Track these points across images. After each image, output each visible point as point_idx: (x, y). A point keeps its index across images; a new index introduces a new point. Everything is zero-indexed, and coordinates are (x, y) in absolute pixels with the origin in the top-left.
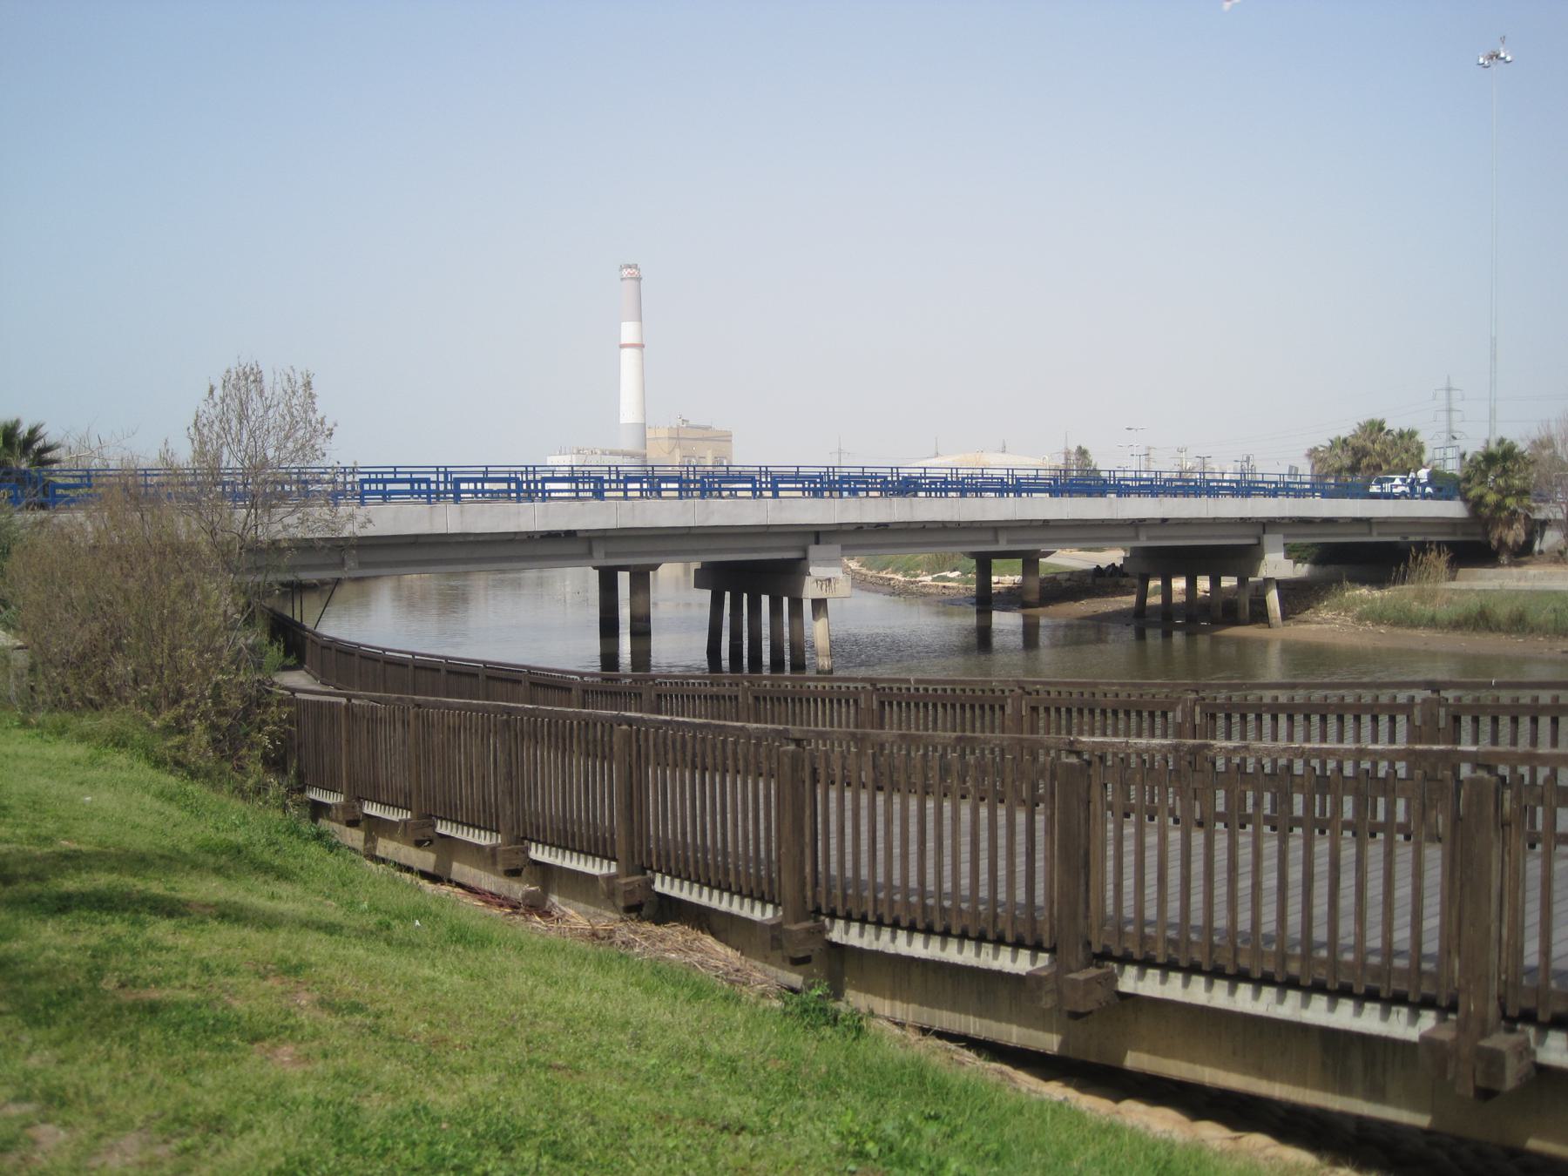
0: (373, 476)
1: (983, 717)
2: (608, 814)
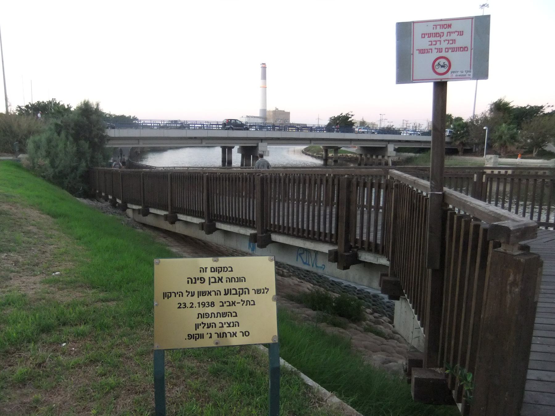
0: (192, 123)
2: (255, 216)
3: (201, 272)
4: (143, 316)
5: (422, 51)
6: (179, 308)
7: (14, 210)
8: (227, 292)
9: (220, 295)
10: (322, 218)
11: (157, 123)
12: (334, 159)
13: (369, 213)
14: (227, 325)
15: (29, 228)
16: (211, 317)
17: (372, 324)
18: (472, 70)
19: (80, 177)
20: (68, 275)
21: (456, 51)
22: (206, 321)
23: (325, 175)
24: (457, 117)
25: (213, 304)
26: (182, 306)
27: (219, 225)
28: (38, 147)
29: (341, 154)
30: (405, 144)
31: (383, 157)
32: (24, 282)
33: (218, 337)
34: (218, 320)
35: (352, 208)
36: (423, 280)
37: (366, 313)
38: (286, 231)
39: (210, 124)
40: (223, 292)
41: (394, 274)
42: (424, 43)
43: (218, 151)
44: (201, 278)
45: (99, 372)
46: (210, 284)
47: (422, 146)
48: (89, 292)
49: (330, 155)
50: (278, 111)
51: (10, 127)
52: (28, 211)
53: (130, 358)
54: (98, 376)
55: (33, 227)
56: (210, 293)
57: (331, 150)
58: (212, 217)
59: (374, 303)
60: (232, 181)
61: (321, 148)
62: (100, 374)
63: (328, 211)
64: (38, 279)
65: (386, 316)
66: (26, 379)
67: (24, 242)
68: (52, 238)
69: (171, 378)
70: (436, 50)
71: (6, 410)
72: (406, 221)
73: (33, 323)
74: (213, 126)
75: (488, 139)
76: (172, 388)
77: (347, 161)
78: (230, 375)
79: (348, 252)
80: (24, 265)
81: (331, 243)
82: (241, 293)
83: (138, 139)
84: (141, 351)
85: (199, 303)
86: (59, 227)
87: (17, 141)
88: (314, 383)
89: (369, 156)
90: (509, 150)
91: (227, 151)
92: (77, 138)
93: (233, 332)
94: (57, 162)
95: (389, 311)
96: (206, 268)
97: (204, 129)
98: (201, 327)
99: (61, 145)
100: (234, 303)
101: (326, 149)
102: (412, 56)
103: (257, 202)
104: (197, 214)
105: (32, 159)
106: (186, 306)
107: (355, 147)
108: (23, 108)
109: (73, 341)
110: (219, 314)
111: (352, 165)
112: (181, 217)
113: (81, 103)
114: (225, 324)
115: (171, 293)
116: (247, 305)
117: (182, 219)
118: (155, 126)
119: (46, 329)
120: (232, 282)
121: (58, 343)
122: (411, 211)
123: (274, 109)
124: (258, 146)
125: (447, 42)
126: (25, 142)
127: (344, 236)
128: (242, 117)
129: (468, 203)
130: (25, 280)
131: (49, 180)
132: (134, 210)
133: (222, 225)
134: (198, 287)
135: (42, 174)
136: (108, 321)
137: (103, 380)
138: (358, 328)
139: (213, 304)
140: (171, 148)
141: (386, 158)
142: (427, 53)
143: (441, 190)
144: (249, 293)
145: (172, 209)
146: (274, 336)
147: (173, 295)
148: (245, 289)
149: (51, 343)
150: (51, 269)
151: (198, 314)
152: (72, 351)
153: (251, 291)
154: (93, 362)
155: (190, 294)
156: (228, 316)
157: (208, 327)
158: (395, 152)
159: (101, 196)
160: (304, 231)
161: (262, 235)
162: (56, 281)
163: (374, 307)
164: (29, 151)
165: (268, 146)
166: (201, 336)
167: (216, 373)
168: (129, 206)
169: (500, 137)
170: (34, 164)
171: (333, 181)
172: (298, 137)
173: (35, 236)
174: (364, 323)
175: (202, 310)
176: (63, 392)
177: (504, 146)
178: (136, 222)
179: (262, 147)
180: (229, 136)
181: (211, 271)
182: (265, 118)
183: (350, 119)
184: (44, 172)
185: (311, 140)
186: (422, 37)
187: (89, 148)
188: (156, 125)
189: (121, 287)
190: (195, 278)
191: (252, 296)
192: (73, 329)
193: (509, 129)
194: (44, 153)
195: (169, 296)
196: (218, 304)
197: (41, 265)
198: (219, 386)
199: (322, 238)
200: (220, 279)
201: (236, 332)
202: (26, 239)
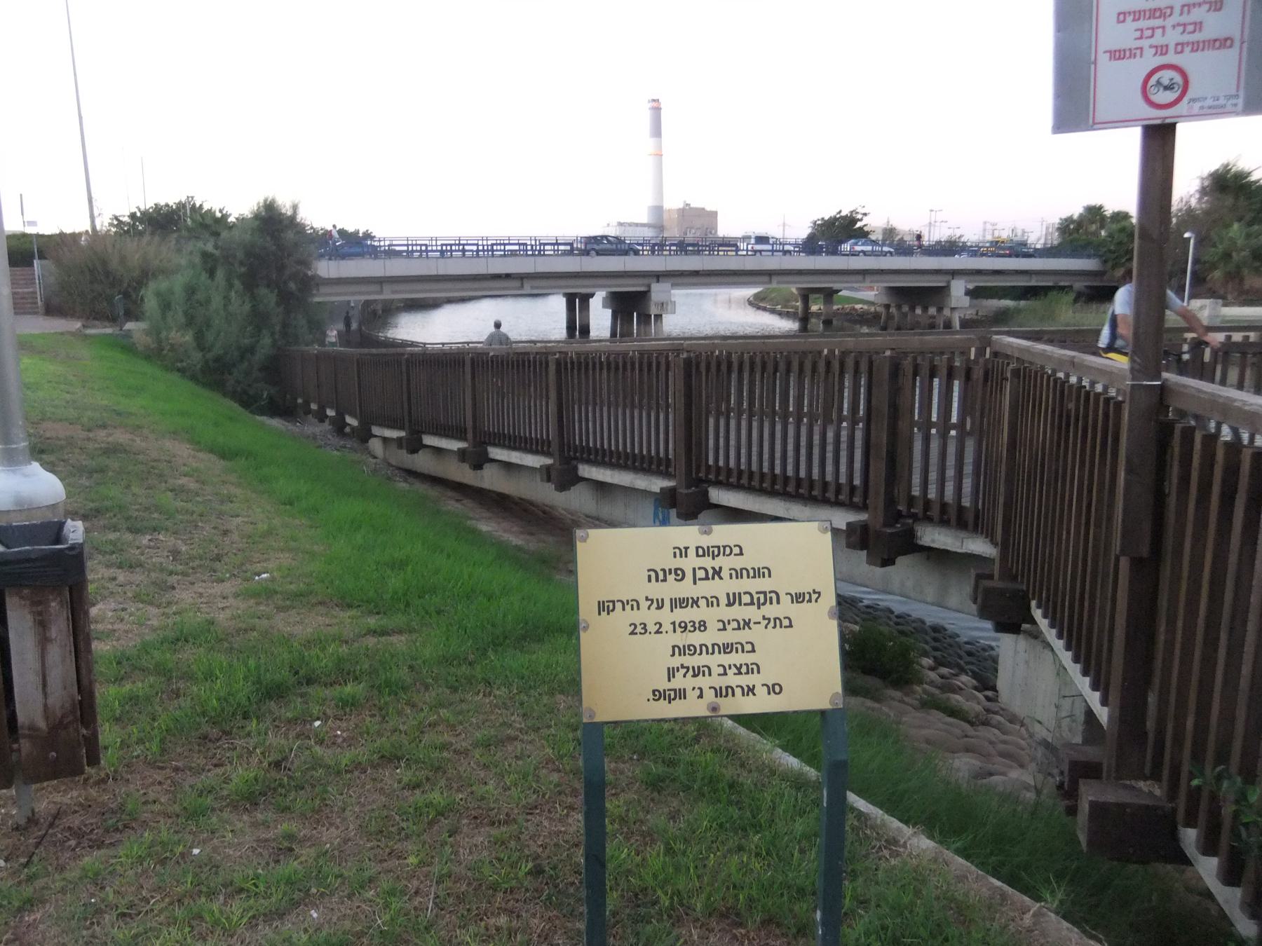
1: (518, 373)
2: (669, 444)
3: (675, 556)
4: (470, 664)
5: (1118, 55)
6: (632, 633)
7: (139, 443)
8: (733, 600)
9: (718, 605)
10: (830, 448)
11: (421, 245)
12: (823, 318)
13: (927, 439)
14: (734, 670)
15: (180, 482)
16: (701, 653)
17: (937, 692)
18: (1242, 93)
19: (260, 370)
20: (289, 579)
21: (1203, 50)
22: (690, 661)
23: (820, 353)
24: (1116, 210)
25: (703, 626)
26: (639, 629)
27: (587, 471)
28: (166, 306)
29: (840, 306)
30: (1014, 278)
31: (940, 309)
32: (201, 595)
33: (716, 696)
34: (715, 660)
35: (902, 425)
36: (1099, 587)
37: (921, 666)
38: (744, 481)
39: (540, 244)
40: (723, 601)
41: (1008, 575)
42: (1123, 35)
43: (557, 304)
44: (676, 570)
45: (405, 780)
46: (695, 583)
47: (1034, 282)
48: (342, 614)
49: (814, 308)
50: (691, 208)
51: (104, 263)
52: (168, 444)
53: (466, 752)
54: (404, 788)
55: (187, 479)
56: (695, 602)
57: (817, 296)
58: (569, 451)
59: (937, 644)
60: (617, 368)
61: (792, 293)
62: (408, 785)
63: (830, 435)
64: (228, 587)
65: (967, 674)
66: (257, 793)
67: (178, 512)
68: (231, 502)
69: (560, 793)
70: (1153, 50)
71: (231, 853)
72: (1043, 454)
73: (245, 678)
74: (547, 247)
75: (1196, 261)
76: (567, 815)
77: (855, 322)
78: (687, 788)
79: (891, 526)
80: (192, 558)
81: (850, 506)
82: (762, 601)
83: (381, 281)
84: (485, 738)
85: (674, 623)
86: (240, 477)
87: (119, 293)
88: (871, 806)
89: (906, 309)
90: (1247, 287)
91: (577, 304)
92: (250, 282)
93: (748, 686)
94: (210, 337)
95: (973, 664)
96: (686, 548)
97: (527, 255)
98: (679, 675)
99: (217, 301)
100: (747, 624)
101: (806, 295)
102: (1093, 66)
103: (673, 418)
104: (534, 447)
105: (155, 331)
106: (646, 631)
107: (871, 289)
108: (126, 219)
109: (336, 718)
110: (716, 647)
111: (865, 330)
112: (497, 453)
113: (258, 204)
114: (730, 668)
115: (613, 602)
116: (775, 627)
117: (498, 457)
118: (417, 251)
119: (276, 692)
120: (742, 577)
121: (304, 720)
122: (1060, 428)
123: (681, 206)
124: (649, 291)
125: (1181, 29)
126: (138, 296)
127: (882, 490)
128: (608, 225)
129: (1236, 404)
130: (201, 590)
131: (193, 378)
132: (385, 440)
133: (594, 469)
134: (671, 589)
135: (179, 365)
136: (403, 674)
137: (418, 797)
138: (906, 699)
139: (703, 626)
140: (450, 301)
141: (946, 312)
142: (1130, 57)
143: (1158, 377)
144: (778, 602)
145: (475, 437)
146: (835, 695)
147: (619, 605)
148: (770, 592)
149: (289, 721)
150: (249, 567)
151: (674, 647)
152: (336, 736)
153: (783, 598)
154: (390, 759)
155: (655, 605)
156: (737, 652)
157: (695, 676)
158: (968, 298)
159: (308, 412)
160: (786, 479)
161: (690, 491)
162: (267, 593)
163: (938, 654)
164: (148, 314)
165: (673, 291)
166: (681, 694)
167: (655, 784)
168: (376, 430)
169: (1227, 256)
170: (159, 341)
171: (842, 364)
172: (742, 268)
173: (198, 499)
174: (918, 689)
175: (681, 639)
176: (338, 820)
177: (1234, 276)
178: (392, 466)
179: (658, 291)
180: (585, 269)
181: (698, 555)
182: (660, 227)
183: (859, 225)
184: (182, 361)
185: (770, 274)
186: (1119, 22)
187: (278, 304)
188: (419, 248)
189: (408, 605)
190: (664, 570)
191: (785, 608)
192: (328, 692)
193: (1248, 236)
194: (183, 320)
195: (611, 608)
196: (713, 626)
197: (226, 559)
198: (666, 810)
199: (830, 495)
200: (717, 573)
201: (754, 686)
202: (179, 504)
